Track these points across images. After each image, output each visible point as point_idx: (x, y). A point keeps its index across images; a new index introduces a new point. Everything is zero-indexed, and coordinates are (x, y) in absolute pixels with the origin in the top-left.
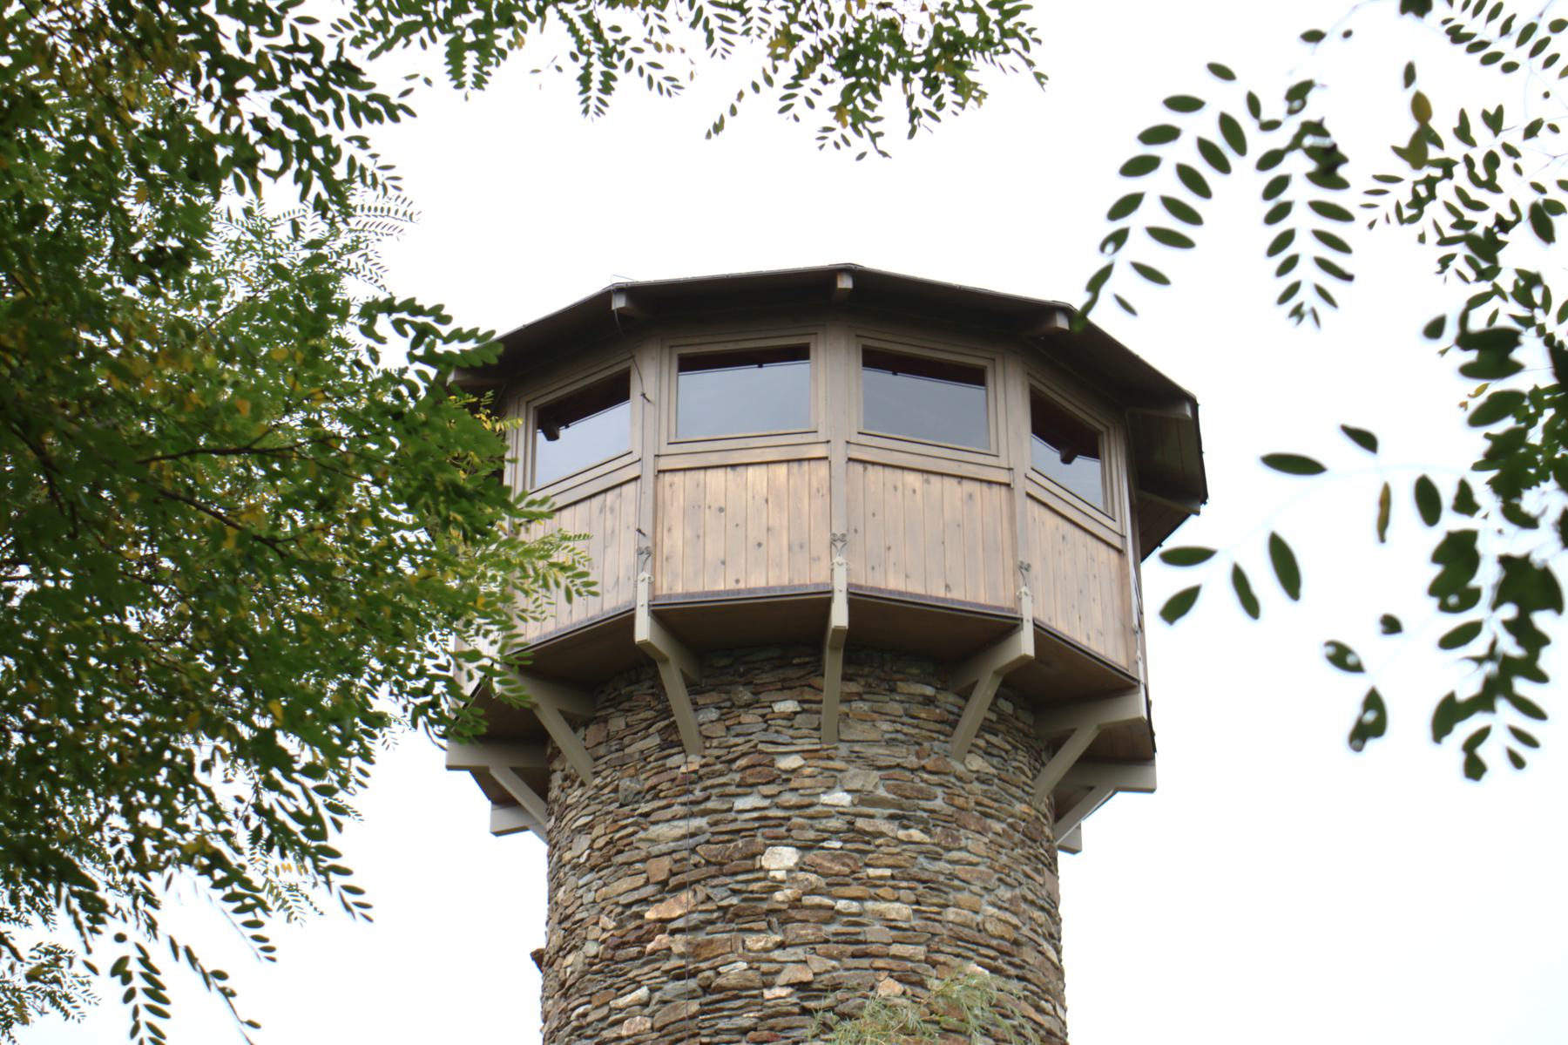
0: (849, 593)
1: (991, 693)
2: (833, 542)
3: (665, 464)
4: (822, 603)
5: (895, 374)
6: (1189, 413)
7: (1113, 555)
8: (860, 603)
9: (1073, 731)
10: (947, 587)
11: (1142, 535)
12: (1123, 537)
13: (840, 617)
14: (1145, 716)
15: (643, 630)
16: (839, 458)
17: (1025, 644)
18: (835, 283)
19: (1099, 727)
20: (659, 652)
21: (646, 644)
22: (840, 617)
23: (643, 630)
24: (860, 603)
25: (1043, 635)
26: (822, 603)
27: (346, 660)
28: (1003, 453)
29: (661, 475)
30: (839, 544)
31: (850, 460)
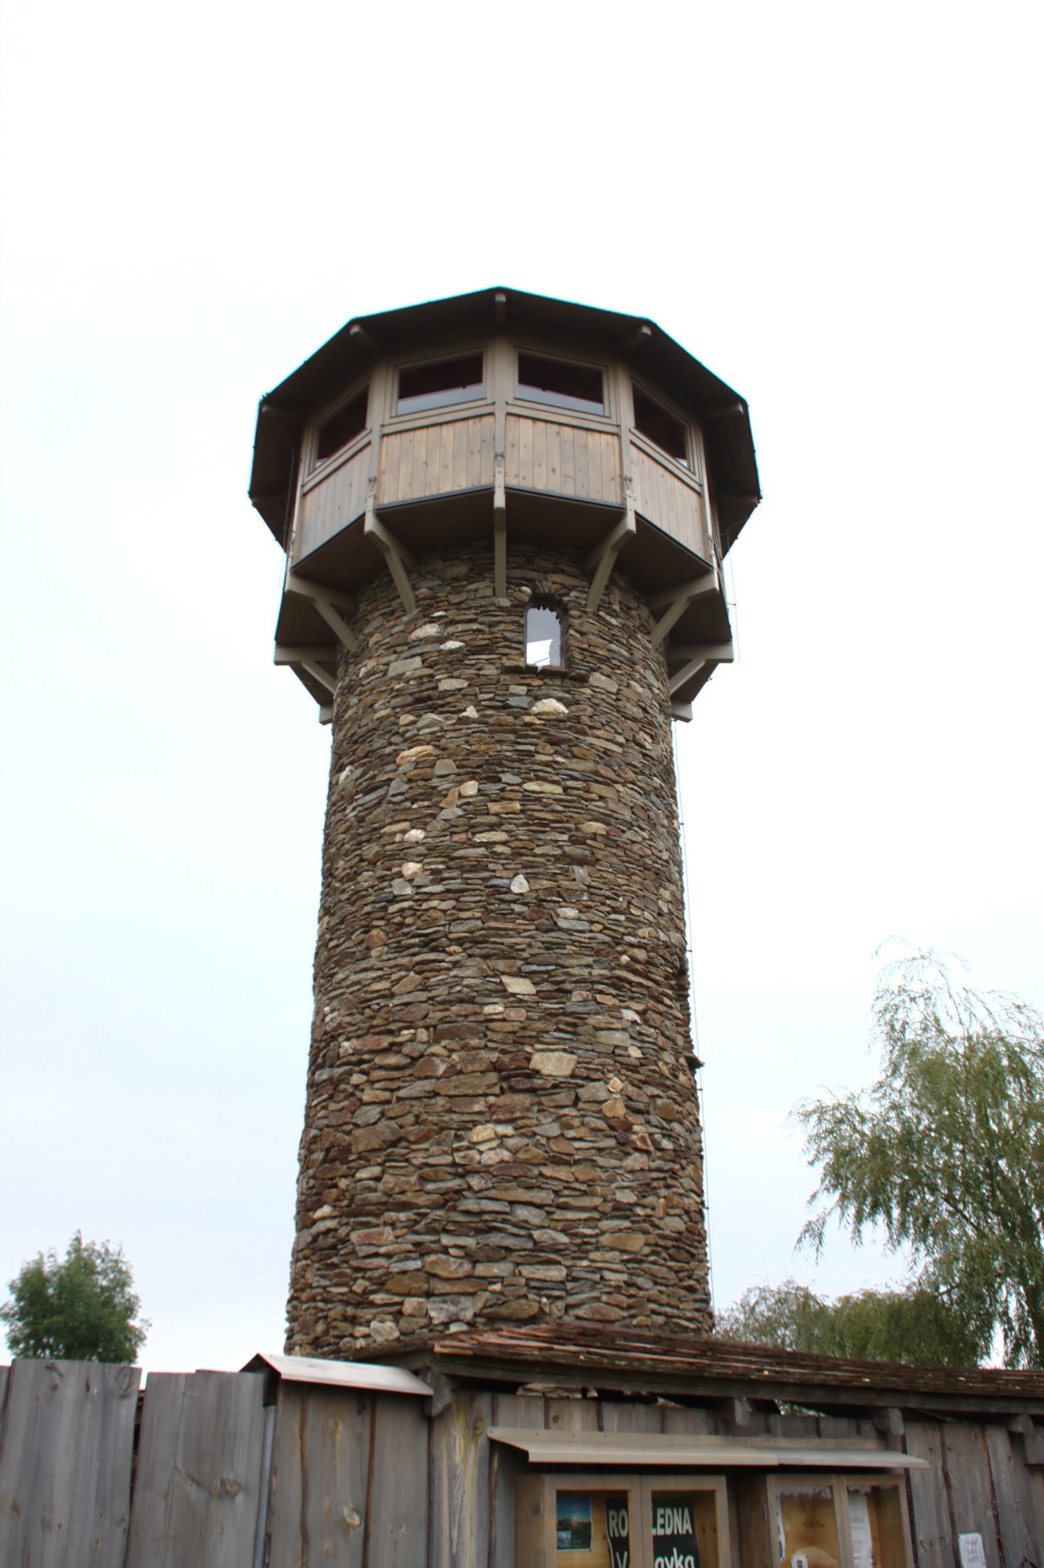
0: (506, 488)
1: (608, 572)
2: (496, 456)
3: (388, 430)
4: (488, 493)
5: (544, 390)
6: (741, 409)
7: (694, 496)
8: (511, 493)
9: (689, 661)
10: (558, 434)
11: (719, 512)
12: (701, 486)
13: (500, 501)
14: (717, 586)
15: (370, 524)
16: (500, 416)
17: (631, 524)
18: (494, 298)
19: (689, 599)
20: (379, 539)
21: (372, 533)
22: (500, 501)
23: (370, 524)
24: (511, 493)
25: (639, 518)
26: (488, 493)
27: (771, 1325)
28: (613, 416)
29: (386, 439)
30: (499, 458)
31: (509, 414)
